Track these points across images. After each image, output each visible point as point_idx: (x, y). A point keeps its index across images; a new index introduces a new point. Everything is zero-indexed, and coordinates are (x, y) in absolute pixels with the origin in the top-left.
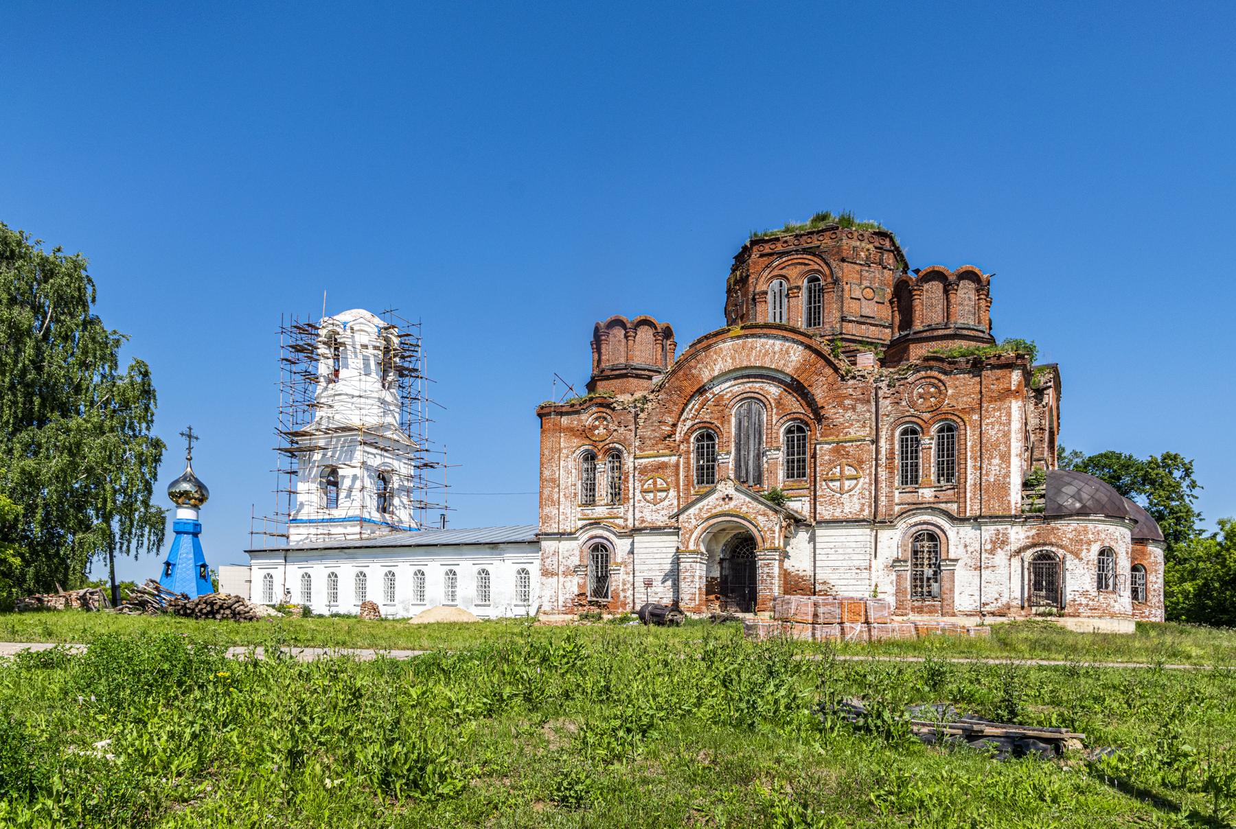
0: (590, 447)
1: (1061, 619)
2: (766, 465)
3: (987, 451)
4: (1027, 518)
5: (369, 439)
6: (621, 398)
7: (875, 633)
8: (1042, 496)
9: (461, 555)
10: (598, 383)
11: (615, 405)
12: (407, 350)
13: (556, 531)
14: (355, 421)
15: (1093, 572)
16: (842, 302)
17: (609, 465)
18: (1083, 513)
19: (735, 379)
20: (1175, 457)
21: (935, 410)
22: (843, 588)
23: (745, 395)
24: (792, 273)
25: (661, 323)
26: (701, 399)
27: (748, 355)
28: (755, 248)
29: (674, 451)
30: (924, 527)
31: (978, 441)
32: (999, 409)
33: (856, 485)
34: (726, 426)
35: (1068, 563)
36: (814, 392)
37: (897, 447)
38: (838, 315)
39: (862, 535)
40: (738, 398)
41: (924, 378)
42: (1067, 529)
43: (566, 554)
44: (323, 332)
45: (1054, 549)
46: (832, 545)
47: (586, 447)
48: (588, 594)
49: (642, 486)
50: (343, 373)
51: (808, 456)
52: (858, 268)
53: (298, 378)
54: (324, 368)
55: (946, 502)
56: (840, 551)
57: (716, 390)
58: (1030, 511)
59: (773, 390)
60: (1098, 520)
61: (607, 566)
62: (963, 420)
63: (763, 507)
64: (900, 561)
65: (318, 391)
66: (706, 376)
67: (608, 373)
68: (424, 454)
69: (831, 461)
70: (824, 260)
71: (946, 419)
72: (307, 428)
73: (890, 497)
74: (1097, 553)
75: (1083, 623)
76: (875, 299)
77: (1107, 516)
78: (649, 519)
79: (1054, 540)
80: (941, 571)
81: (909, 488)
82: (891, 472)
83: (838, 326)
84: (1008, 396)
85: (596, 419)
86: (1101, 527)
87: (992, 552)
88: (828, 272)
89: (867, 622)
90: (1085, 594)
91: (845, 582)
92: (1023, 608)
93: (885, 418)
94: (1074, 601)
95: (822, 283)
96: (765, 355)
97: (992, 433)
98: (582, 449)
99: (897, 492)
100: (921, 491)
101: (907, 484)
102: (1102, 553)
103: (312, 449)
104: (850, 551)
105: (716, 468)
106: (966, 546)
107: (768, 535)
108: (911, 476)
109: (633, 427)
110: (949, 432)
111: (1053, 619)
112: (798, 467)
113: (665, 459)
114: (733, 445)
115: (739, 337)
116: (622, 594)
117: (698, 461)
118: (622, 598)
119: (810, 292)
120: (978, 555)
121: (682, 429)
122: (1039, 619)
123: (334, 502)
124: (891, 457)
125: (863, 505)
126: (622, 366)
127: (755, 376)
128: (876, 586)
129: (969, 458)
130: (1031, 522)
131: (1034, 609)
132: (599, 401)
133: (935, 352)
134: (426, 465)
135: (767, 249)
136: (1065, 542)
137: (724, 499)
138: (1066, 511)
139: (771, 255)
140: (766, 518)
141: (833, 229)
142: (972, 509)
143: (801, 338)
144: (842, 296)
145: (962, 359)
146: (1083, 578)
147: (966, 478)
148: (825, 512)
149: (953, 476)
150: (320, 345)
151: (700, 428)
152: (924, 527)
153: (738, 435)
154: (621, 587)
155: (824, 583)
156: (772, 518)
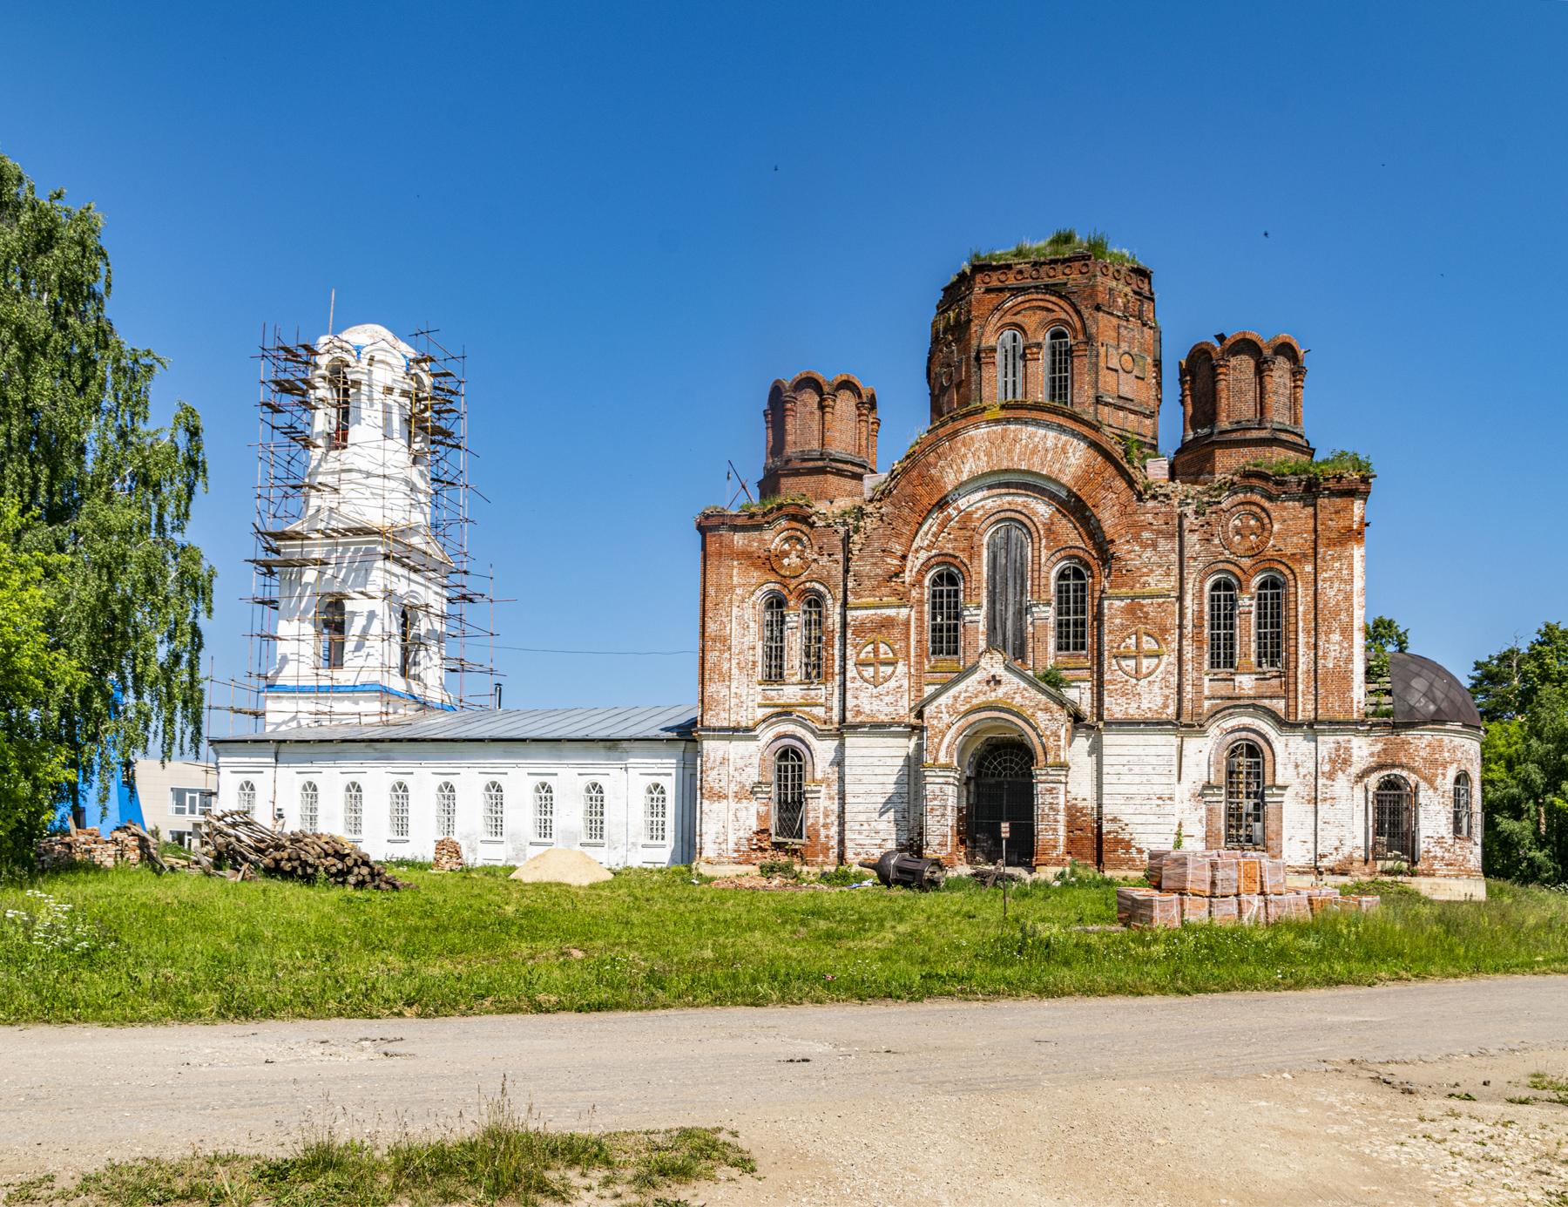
0: (777, 587)
1: (1414, 880)
2: (1030, 629)
3: (1324, 620)
4: (1374, 725)
5: (397, 550)
6: (821, 507)
7: (1272, 909)
8: (1389, 693)
9: (560, 757)
10: (783, 480)
11: (814, 518)
12: (443, 398)
13: (725, 724)
14: (374, 518)
15: (1448, 808)
16: (1097, 373)
17: (803, 617)
18: (1438, 720)
19: (990, 487)
20: (1390, 624)
21: (1255, 553)
22: (1140, 829)
23: (1002, 515)
24: (1031, 321)
25: (865, 389)
26: (941, 516)
27: (1009, 451)
28: (978, 277)
29: (903, 599)
30: (1244, 734)
31: (1312, 605)
32: (1339, 559)
33: (1157, 666)
34: (976, 562)
35: (1421, 794)
36: (1100, 516)
37: (1207, 608)
38: (1091, 393)
39: (1164, 743)
40: (992, 519)
41: (1242, 503)
42: (1420, 741)
43: (741, 763)
44: (323, 361)
45: (1404, 773)
46: (1124, 760)
47: (771, 586)
48: (773, 831)
49: (858, 654)
50: (355, 433)
51: (1089, 617)
52: (1115, 321)
53: (279, 437)
54: (323, 421)
55: (1271, 698)
56: (1136, 769)
57: (962, 503)
58: (1374, 714)
59: (1042, 510)
60: (1455, 732)
61: (800, 785)
62: (1293, 572)
63: (1044, 698)
64: (1213, 787)
65: (314, 463)
66: (950, 480)
67: (797, 464)
68: (465, 580)
69: (1124, 627)
70: (1074, 306)
71: (1271, 569)
72: (297, 526)
73: (1197, 686)
74: (1453, 781)
75: (1439, 885)
76: (1135, 373)
77: (1464, 725)
78: (867, 708)
79: (1404, 760)
80: (1265, 804)
81: (1223, 672)
82: (1200, 648)
83: (1091, 410)
84: (1349, 539)
85: (786, 540)
86: (1458, 740)
87: (1331, 776)
88: (1078, 325)
89: (1262, 893)
90: (1440, 841)
91: (1142, 819)
92: (1366, 861)
93: (1192, 563)
94: (1428, 852)
95: (1070, 341)
96: (1033, 453)
97: (1330, 593)
98: (765, 588)
99: (1206, 679)
100: (1238, 678)
101: (1219, 667)
102: (1457, 781)
103: (303, 564)
104: (1149, 769)
105: (961, 630)
106: (1297, 766)
107: (1051, 743)
108: (1223, 655)
109: (839, 556)
110: (1274, 587)
111: (1406, 879)
112: (1072, 635)
113: (891, 612)
114: (984, 593)
115: (997, 421)
116: (823, 832)
117: (934, 618)
118: (823, 839)
119: (1054, 354)
120: (1313, 780)
121: (915, 563)
122: (1387, 879)
123: (334, 657)
124: (1198, 626)
125: (1167, 697)
126: (816, 454)
127: (1018, 486)
128: (1180, 825)
129: (1300, 629)
130: (1378, 732)
131: (1380, 863)
132: (791, 510)
133: (1256, 466)
134: (464, 597)
135: (994, 280)
136: (1418, 763)
137: (988, 682)
138: (1418, 717)
139: (1001, 290)
140: (1048, 716)
141: (1084, 257)
142: (1305, 711)
143: (1085, 430)
144: (1096, 365)
145: (1293, 479)
146: (1439, 817)
147: (1297, 662)
148: (1115, 707)
149: (1278, 656)
150: (318, 382)
151: (938, 564)
152: (1244, 734)
153: (992, 579)
154: (821, 821)
155: (1114, 820)
156: (1057, 715)
